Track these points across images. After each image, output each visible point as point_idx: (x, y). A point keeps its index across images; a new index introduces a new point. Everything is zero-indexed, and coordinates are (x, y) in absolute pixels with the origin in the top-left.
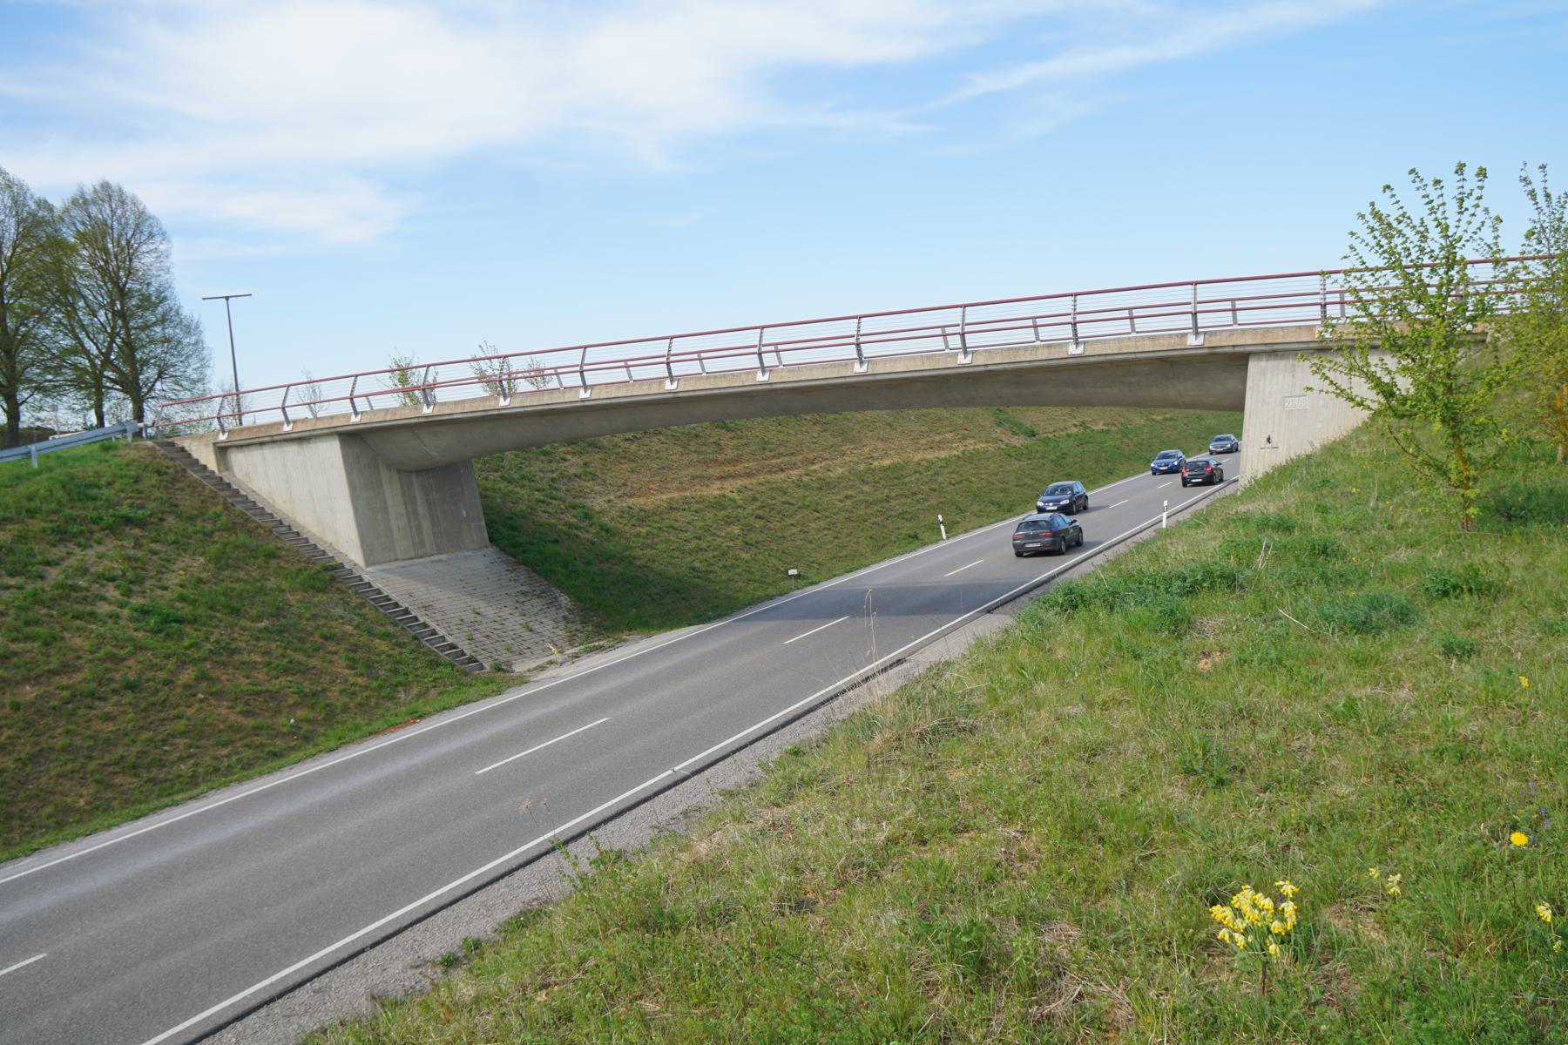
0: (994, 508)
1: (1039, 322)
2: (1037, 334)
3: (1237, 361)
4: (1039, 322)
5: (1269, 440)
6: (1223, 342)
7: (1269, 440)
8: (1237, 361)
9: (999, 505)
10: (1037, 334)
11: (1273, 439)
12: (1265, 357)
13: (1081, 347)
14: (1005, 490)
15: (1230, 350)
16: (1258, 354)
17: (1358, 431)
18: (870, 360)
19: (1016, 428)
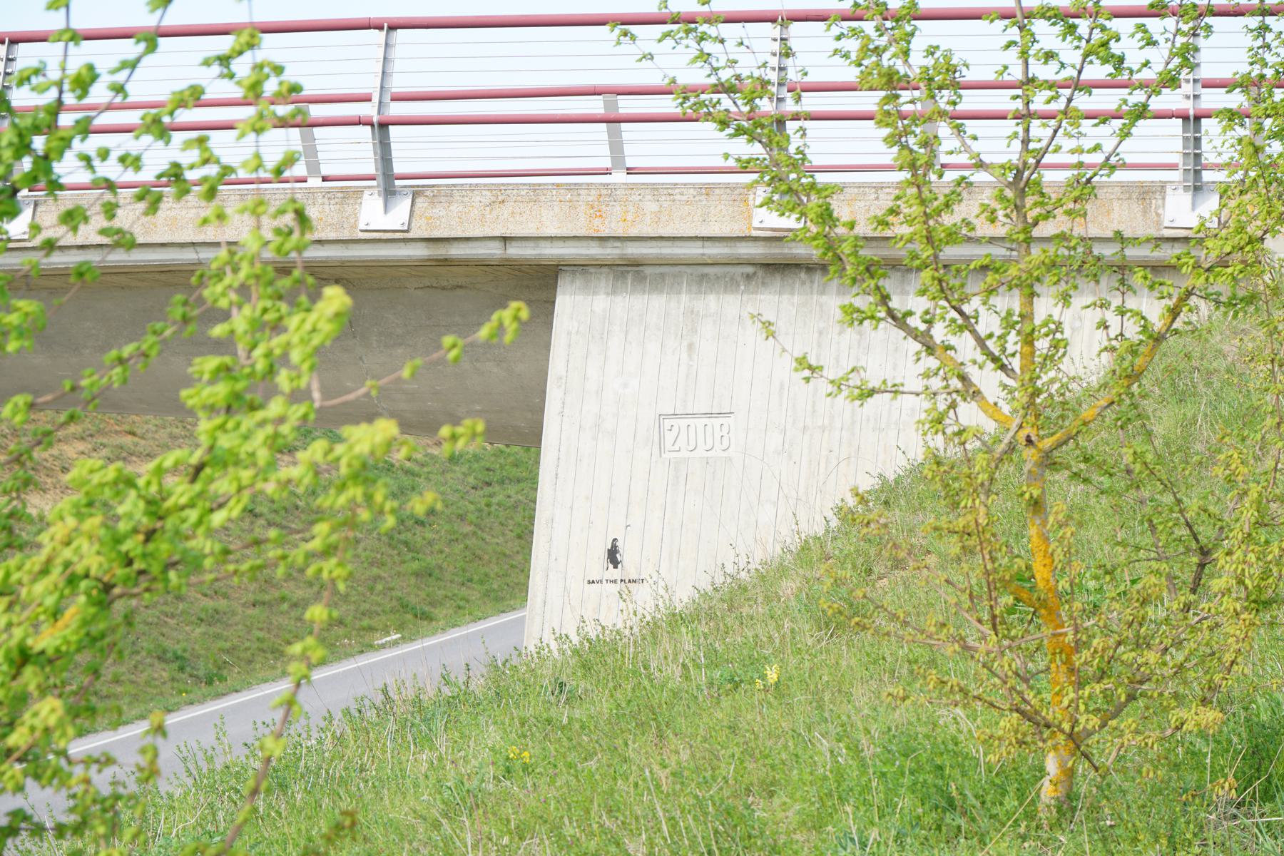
0: (164, 672)
1: (628, 105)
2: (616, 147)
3: (536, 281)
4: (628, 105)
5: (613, 556)
6: (472, 221)
7: (613, 556)
8: (536, 281)
9: (182, 662)
10: (616, 147)
11: (625, 555)
12: (604, 280)
13: (402, 207)
14: (214, 618)
15: (493, 251)
16: (582, 268)
17: (873, 530)
18: (424, 187)
19: (66, 489)
